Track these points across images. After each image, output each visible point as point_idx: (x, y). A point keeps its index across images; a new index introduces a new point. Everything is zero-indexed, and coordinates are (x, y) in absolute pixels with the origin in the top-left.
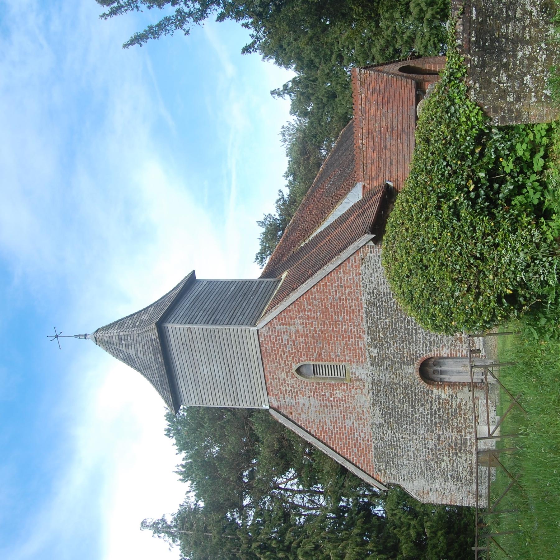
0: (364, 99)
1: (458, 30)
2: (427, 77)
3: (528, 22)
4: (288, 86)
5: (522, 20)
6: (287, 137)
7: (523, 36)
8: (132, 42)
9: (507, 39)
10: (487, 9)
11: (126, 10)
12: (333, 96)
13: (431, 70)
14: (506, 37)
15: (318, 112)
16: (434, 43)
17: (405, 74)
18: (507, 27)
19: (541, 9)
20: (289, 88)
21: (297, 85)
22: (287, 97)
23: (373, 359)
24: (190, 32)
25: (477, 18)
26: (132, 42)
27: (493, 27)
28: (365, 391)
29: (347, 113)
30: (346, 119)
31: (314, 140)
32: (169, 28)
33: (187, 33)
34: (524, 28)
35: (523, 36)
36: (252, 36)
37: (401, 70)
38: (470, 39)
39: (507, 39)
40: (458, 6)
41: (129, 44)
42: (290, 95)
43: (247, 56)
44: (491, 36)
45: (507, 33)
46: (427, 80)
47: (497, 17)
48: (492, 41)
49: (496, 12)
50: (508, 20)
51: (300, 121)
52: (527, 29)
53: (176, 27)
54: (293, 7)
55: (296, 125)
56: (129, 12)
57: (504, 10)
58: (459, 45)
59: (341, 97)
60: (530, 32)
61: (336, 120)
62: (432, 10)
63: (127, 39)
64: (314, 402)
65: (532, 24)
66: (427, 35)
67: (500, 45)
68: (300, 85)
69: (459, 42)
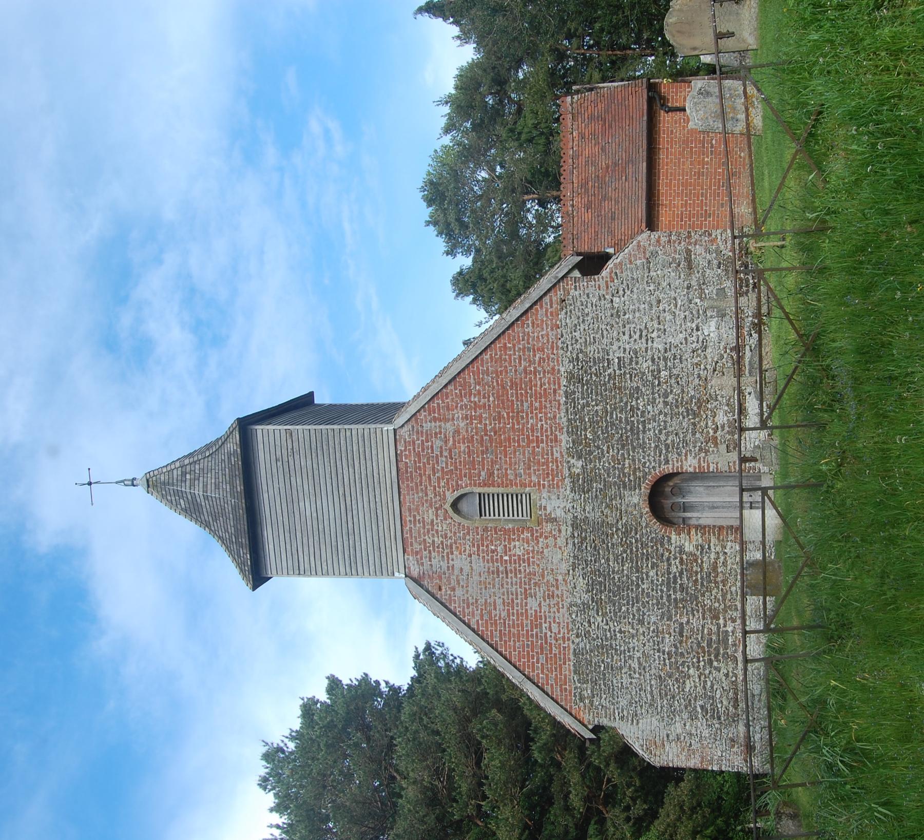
23: (574, 478)
28: (561, 541)
64: (479, 565)
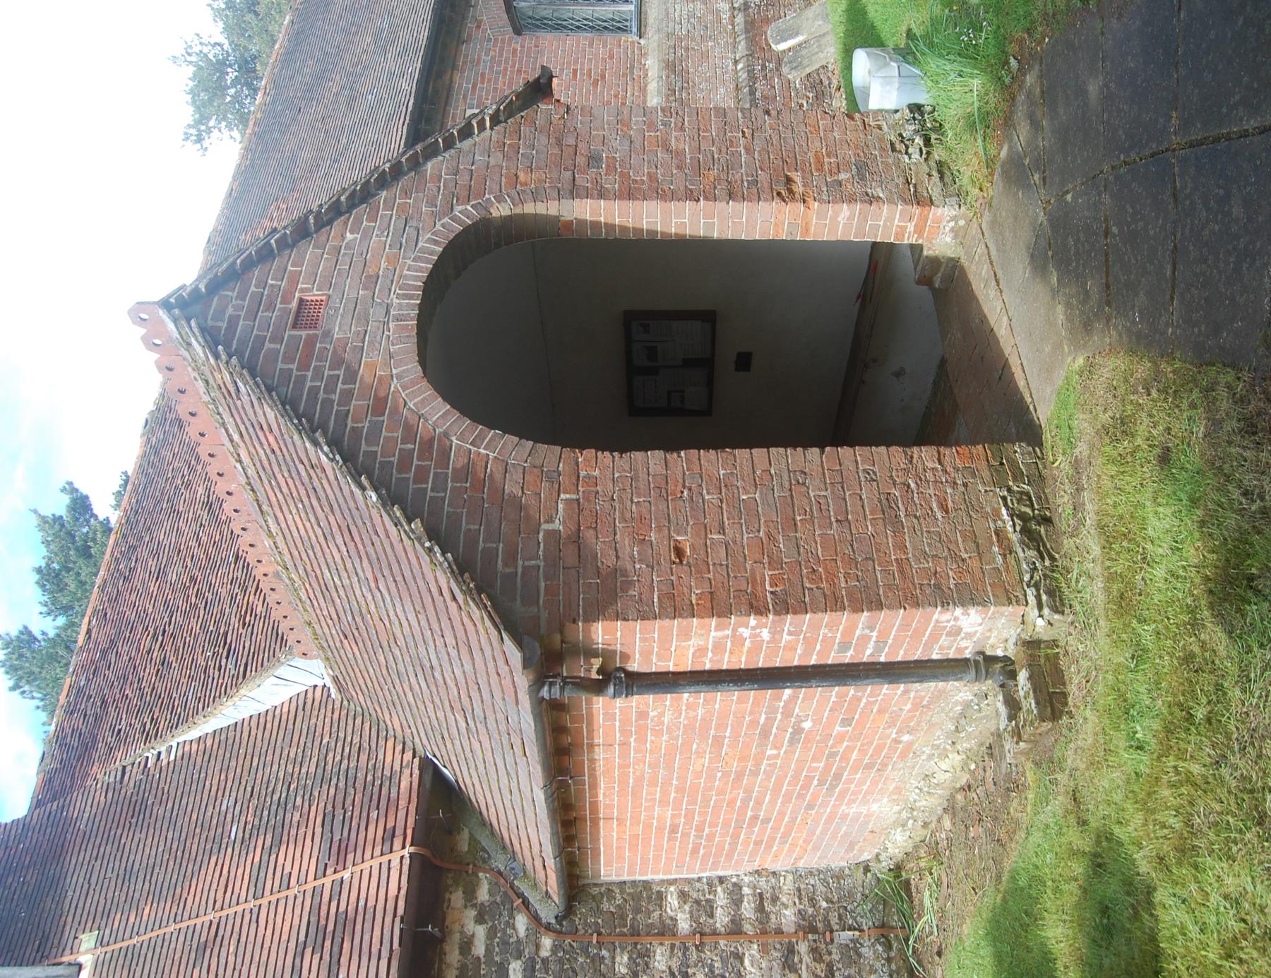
13: (610, 227)
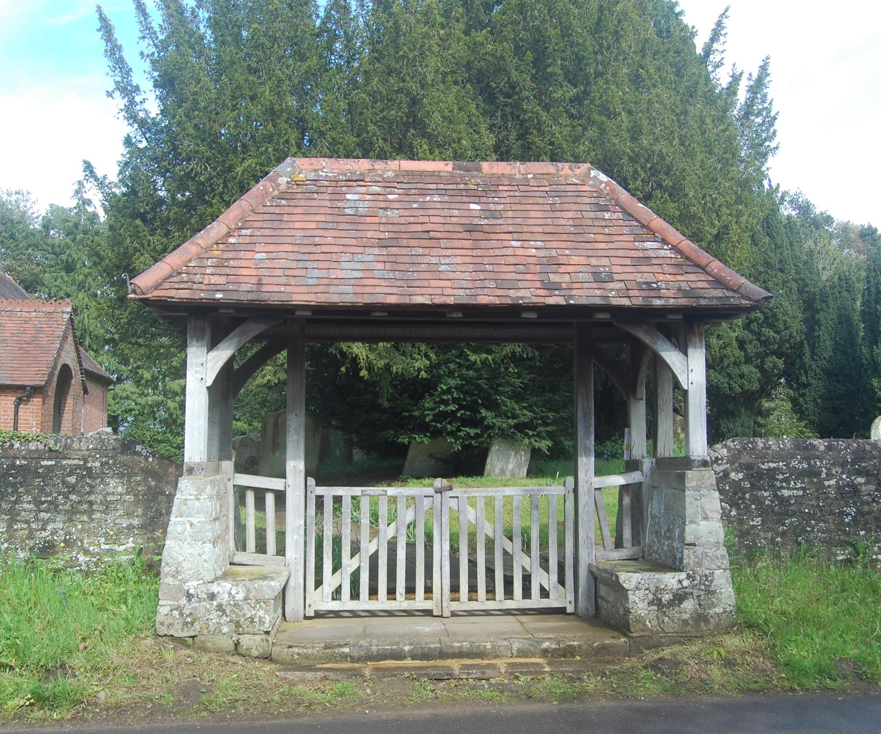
0: (28, 315)
1: (31, 444)
2: (51, 402)
3: (34, 526)
4: (89, 205)
5: (37, 519)
6: (14, 198)
7: (18, 521)
8: (103, 19)
9: (15, 502)
10: (51, 479)
11: (141, 22)
12: (69, 268)
14: (18, 501)
15: (48, 245)
16: (131, 410)
17: (57, 372)
18: (29, 502)
19: (48, 542)
20: (87, 207)
21: (88, 220)
22: (73, 203)
24: (110, 98)
25: (42, 467)
26: (103, 19)
27: (31, 485)
29: (43, 285)
30: (31, 285)
31: (7, 235)
32: (117, 72)
33: (110, 94)
34: (27, 522)
35: (18, 521)
36: (105, 177)
37: (66, 369)
38: (18, 458)
39: (15, 502)
40: (59, 444)
41: (101, 15)
42: (75, 208)
43: (81, 166)
44: (20, 483)
45: (22, 502)
46: (46, 402)
47: (42, 490)
48: (14, 485)
49: (48, 489)
50: (37, 503)
51: (37, 218)
52: (26, 526)
53: (117, 83)
54: (131, 236)
55: (31, 211)
56: (138, 26)
57: (49, 499)
58: (13, 445)
59: (66, 279)
60: (22, 529)
61: (33, 269)
62: (175, 408)
63: (107, 12)
65: (31, 531)
66: (143, 401)
67: (9, 494)
68: (88, 222)
69: (17, 445)
